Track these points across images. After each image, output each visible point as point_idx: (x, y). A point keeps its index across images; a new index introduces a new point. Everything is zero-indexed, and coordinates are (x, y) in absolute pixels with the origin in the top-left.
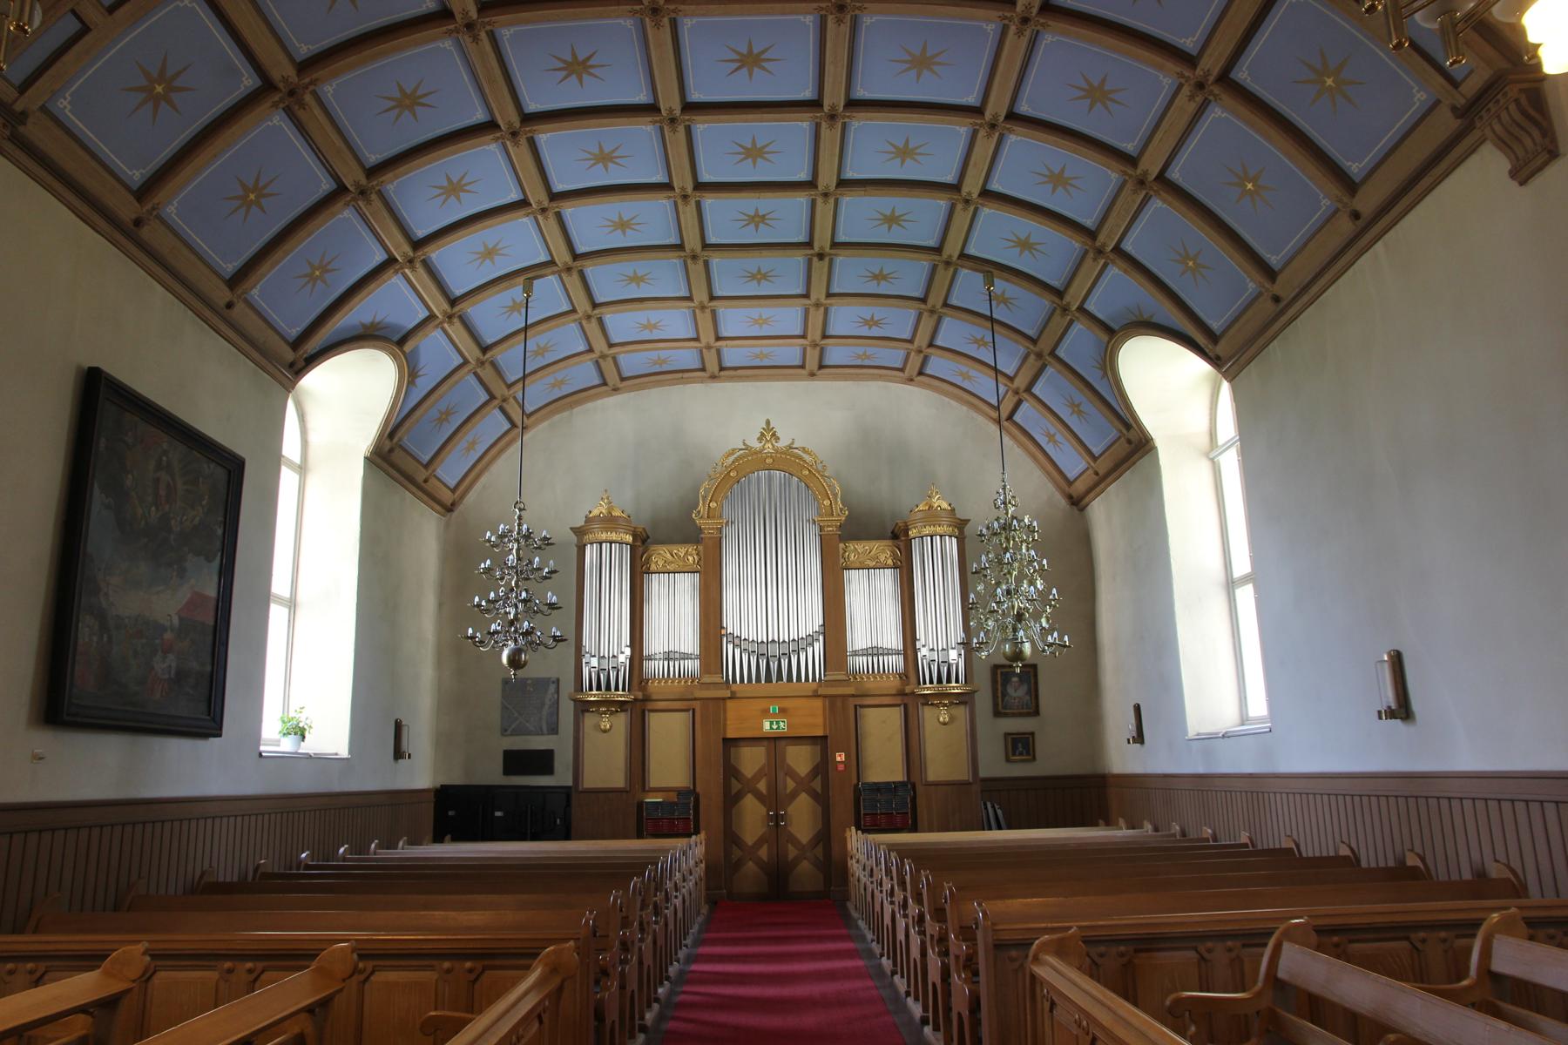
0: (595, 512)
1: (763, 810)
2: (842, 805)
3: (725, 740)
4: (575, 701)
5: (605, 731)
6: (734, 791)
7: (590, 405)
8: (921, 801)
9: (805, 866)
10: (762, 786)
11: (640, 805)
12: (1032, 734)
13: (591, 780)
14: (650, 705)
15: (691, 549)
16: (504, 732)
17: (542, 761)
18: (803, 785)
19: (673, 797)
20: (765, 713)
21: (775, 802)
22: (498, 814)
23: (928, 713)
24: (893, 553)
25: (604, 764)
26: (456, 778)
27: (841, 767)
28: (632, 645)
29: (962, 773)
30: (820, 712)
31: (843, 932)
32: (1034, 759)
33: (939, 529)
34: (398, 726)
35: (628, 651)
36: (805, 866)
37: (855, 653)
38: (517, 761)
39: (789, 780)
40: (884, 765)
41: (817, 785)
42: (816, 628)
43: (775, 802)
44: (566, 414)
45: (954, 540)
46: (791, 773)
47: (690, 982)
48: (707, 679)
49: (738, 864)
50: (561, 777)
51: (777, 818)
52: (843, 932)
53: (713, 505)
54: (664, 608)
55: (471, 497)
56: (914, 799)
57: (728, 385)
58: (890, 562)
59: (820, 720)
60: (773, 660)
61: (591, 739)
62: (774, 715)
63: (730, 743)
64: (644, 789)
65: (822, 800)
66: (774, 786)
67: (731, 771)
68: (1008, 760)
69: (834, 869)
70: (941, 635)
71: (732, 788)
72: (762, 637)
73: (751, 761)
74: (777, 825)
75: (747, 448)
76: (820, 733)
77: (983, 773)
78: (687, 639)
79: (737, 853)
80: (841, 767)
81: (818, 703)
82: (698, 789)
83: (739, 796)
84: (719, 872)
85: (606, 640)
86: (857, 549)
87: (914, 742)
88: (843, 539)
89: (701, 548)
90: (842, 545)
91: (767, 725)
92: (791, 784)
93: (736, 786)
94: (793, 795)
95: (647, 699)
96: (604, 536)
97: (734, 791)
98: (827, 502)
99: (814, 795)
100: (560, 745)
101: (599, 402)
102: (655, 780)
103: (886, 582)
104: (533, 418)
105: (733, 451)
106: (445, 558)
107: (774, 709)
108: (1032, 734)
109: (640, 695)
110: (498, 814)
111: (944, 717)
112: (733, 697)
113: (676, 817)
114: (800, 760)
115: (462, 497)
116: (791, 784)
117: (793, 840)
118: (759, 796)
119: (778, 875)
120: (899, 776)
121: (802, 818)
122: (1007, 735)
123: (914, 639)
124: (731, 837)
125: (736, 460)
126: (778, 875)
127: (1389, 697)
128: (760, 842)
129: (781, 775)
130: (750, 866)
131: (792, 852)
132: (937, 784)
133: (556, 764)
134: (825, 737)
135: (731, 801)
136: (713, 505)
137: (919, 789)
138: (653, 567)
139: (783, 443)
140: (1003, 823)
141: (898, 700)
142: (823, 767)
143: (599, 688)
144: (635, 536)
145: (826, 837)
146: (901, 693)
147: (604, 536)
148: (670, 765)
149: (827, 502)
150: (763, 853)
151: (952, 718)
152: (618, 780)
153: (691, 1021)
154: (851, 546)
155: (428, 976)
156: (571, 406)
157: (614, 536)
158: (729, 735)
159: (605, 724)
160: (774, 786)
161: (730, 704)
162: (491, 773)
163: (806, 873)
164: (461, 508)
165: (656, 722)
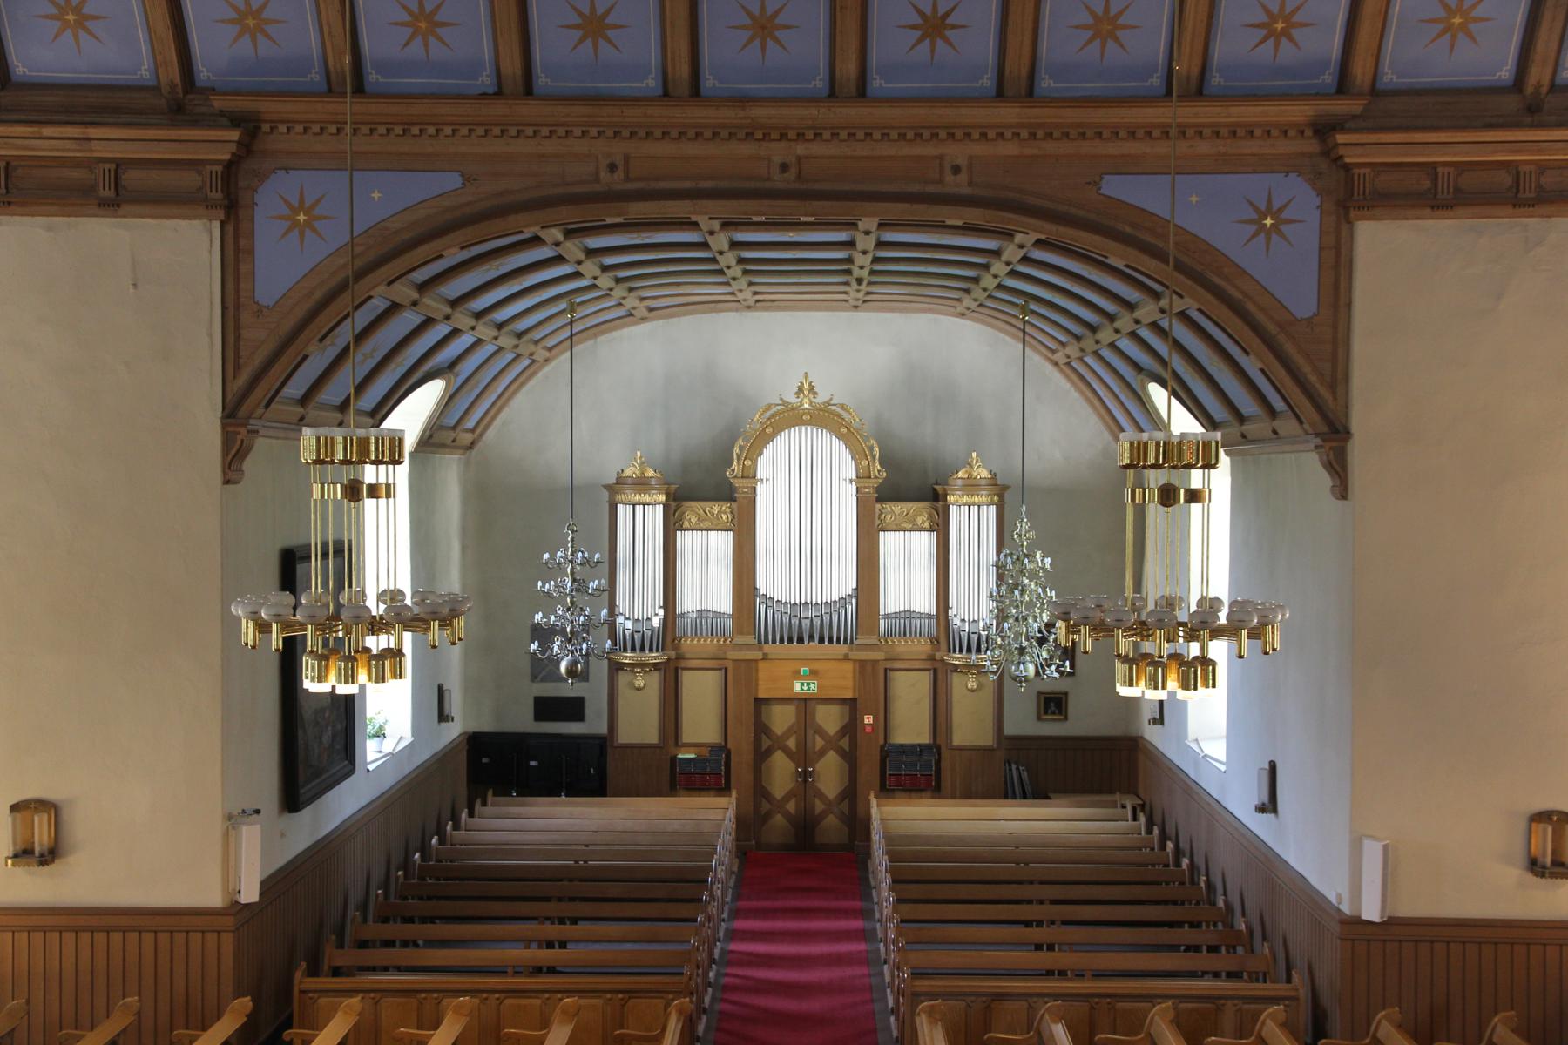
0: (628, 473)
1: (792, 766)
2: (869, 770)
3: (757, 700)
4: (609, 659)
5: (639, 689)
6: (764, 747)
7: (616, 334)
8: (945, 764)
9: (831, 820)
10: (792, 743)
11: (674, 759)
12: (1066, 694)
13: (625, 736)
14: (683, 664)
15: (725, 506)
16: (534, 678)
17: (573, 708)
18: (831, 743)
19: (705, 752)
20: (797, 674)
21: (804, 758)
22: (533, 763)
23: (956, 679)
24: (931, 515)
25: (638, 723)
26: (486, 725)
27: (868, 730)
28: (665, 607)
29: (986, 739)
30: (850, 675)
31: (857, 904)
32: (1066, 718)
33: (976, 499)
34: (440, 688)
35: (661, 612)
36: (831, 820)
37: (887, 616)
38: (547, 708)
39: (818, 738)
40: (911, 727)
41: (845, 806)
42: (849, 592)
43: (804, 758)
44: (590, 343)
45: (993, 508)
46: (820, 731)
47: (740, 964)
48: (739, 640)
49: (768, 816)
50: (594, 724)
51: (805, 774)
52: (857, 904)
53: (748, 463)
54: (697, 574)
55: (491, 434)
56: (938, 762)
57: (766, 314)
58: (927, 525)
59: (850, 683)
60: (806, 631)
61: (625, 696)
62: (805, 677)
63: (760, 702)
64: (676, 744)
65: (850, 758)
66: (803, 744)
67: (761, 728)
68: (1039, 718)
69: (858, 826)
70: (972, 605)
71: (763, 743)
72: (795, 599)
73: (781, 719)
74: (805, 781)
75: (784, 403)
76: (849, 695)
77: (1009, 730)
78: (721, 600)
79: (766, 806)
80: (868, 730)
81: (849, 666)
82: (729, 746)
83: (768, 753)
84: (748, 826)
85: (638, 604)
86: (897, 509)
87: (941, 719)
88: (879, 500)
89: (735, 505)
90: (878, 506)
91: (797, 686)
92: (820, 743)
93: (766, 743)
94: (822, 753)
95: (680, 658)
96: (637, 498)
97: (764, 747)
98: (864, 463)
99: (842, 754)
100: (595, 694)
101: (625, 331)
102: (688, 736)
103: (924, 542)
104: (554, 351)
105: (770, 406)
106: (466, 500)
107: (805, 670)
108: (1066, 694)
109: (673, 654)
110: (533, 763)
111: (972, 684)
112: (765, 658)
113: (707, 775)
114: (830, 719)
115: (481, 435)
116: (820, 743)
117: (820, 794)
118: (786, 751)
119: (805, 826)
120: (925, 739)
121: (829, 775)
122: (1040, 693)
123: (947, 607)
124: (760, 791)
125: (772, 416)
126: (805, 826)
127: (1265, 798)
128: (787, 798)
129: (810, 732)
130: (779, 819)
131: (819, 806)
132: (960, 749)
133: (588, 711)
134: (854, 700)
135: (761, 756)
136: (748, 463)
137: (945, 754)
138: (686, 524)
139: (820, 399)
140: (1028, 789)
141: (927, 665)
142: (851, 728)
143: (633, 649)
144: (668, 495)
145: (851, 794)
146: (932, 658)
147: (637, 498)
148: (701, 723)
149: (864, 463)
150: (791, 806)
151: (980, 686)
152: (652, 737)
153: (745, 1005)
154: (888, 506)
155: (598, 1002)
156: (595, 336)
157: (647, 498)
158: (761, 695)
159: (640, 682)
160: (803, 744)
161: (761, 665)
162: (523, 721)
163: (832, 827)
164: (480, 445)
165: (687, 678)
